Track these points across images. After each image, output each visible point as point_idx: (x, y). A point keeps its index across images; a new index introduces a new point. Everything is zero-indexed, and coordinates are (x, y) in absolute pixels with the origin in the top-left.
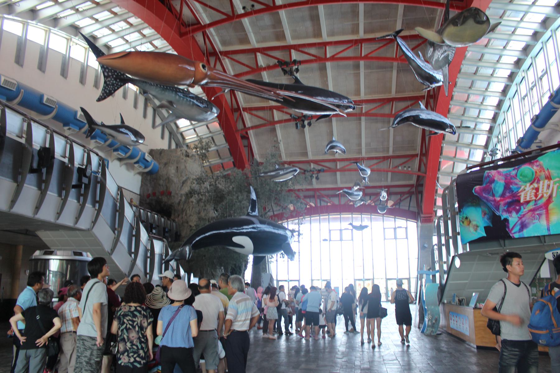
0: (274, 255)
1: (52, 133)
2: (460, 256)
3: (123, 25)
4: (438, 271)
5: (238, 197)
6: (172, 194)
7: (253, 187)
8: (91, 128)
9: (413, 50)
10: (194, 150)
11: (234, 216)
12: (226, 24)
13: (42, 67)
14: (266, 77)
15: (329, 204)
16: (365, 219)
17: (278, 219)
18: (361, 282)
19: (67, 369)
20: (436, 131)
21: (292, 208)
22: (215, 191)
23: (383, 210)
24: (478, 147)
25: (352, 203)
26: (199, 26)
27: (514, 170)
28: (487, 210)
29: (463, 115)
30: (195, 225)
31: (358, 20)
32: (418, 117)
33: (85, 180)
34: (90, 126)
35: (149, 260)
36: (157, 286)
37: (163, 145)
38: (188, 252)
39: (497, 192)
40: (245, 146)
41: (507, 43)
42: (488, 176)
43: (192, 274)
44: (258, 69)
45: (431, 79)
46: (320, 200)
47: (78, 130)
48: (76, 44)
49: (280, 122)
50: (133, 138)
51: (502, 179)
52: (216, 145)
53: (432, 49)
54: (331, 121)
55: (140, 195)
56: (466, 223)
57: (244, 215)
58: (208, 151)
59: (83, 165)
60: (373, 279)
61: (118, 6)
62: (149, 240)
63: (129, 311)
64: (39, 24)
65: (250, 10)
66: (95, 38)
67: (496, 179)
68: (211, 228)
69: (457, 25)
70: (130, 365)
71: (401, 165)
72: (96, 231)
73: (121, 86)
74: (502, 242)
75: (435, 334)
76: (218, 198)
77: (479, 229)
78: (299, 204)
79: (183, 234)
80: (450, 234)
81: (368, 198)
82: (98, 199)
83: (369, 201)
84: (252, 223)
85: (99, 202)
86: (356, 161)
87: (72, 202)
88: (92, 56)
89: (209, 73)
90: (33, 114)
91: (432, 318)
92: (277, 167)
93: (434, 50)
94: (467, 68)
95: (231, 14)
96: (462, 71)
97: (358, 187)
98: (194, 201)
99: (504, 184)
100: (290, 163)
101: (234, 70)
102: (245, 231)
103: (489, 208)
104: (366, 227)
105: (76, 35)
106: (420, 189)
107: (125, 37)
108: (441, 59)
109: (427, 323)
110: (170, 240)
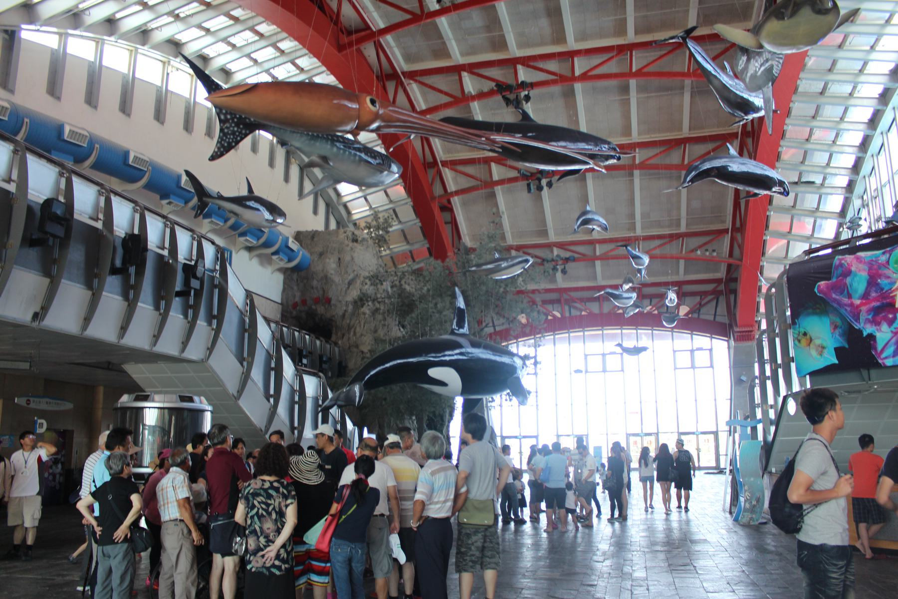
0: (497, 397)
1: (142, 211)
2: (795, 396)
3: (249, 36)
4: (760, 421)
5: (436, 304)
6: (333, 302)
7: (459, 288)
8: (202, 200)
9: (714, 59)
10: (366, 231)
11: (432, 336)
12: (412, 28)
13: (125, 107)
14: (478, 112)
15: (583, 313)
16: (642, 337)
17: (501, 339)
18: (638, 439)
19: (172, 576)
20: (757, 191)
21: (524, 321)
22: (400, 295)
23: (671, 321)
24: (829, 215)
25: (621, 311)
26: (368, 32)
27: (884, 253)
28: (838, 321)
29: (802, 162)
30: (370, 351)
31: (625, 13)
32: (727, 166)
33: (195, 284)
34: (200, 200)
35: (297, 407)
36: (310, 448)
37: (317, 223)
38: (358, 394)
39: (856, 291)
40: (446, 223)
41: (877, 40)
42: (841, 265)
43: (366, 429)
44: (463, 99)
45: (746, 107)
47: (183, 205)
48: (177, 69)
49: (501, 182)
50: (267, 215)
51: (864, 270)
52: (400, 222)
53: (745, 58)
54: (584, 179)
55: (281, 304)
56: (804, 342)
57: (446, 333)
58: (388, 232)
59: (191, 260)
60: (657, 434)
61: (240, 6)
63: (261, 488)
64: (119, 41)
66: (205, 59)
67: (853, 269)
68: (398, 354)
69: (783, 19)
70: (265, 571)
71: (700, 247)
72: (212, 362)
73: (246, 135)
74: (865, 373)
75: (757, 523)
76: (405, 306)
77: (825, 351)
78: (535, 314)
79: (351, 365)
80: (779, 361)
81: (647, 301)
82: (215, 312)
83: (649, 308)
84: (459, 346)
85: (217, 318)
86: (627, 242)
87: (176, 318)
88: (202, 93)
89: (381, 112)
90: (114, 183)
91: (751, 497)
92: (497, 255)
93: (748, 60)
94: (807, 84)
95: (418, 12)
96: (800, 90)
97: (630, 285)
98: (368, 312)
99: (867, 277)
100: (518, 248)
101: (425, 101)
102: (447, 358)
103: (843, 318)
104: (644, 349)
105: (176, 57)
106: (732, 285)
107: (252, 55)
108: (759, 73)
109: (743, 504)
110: (330, 374)
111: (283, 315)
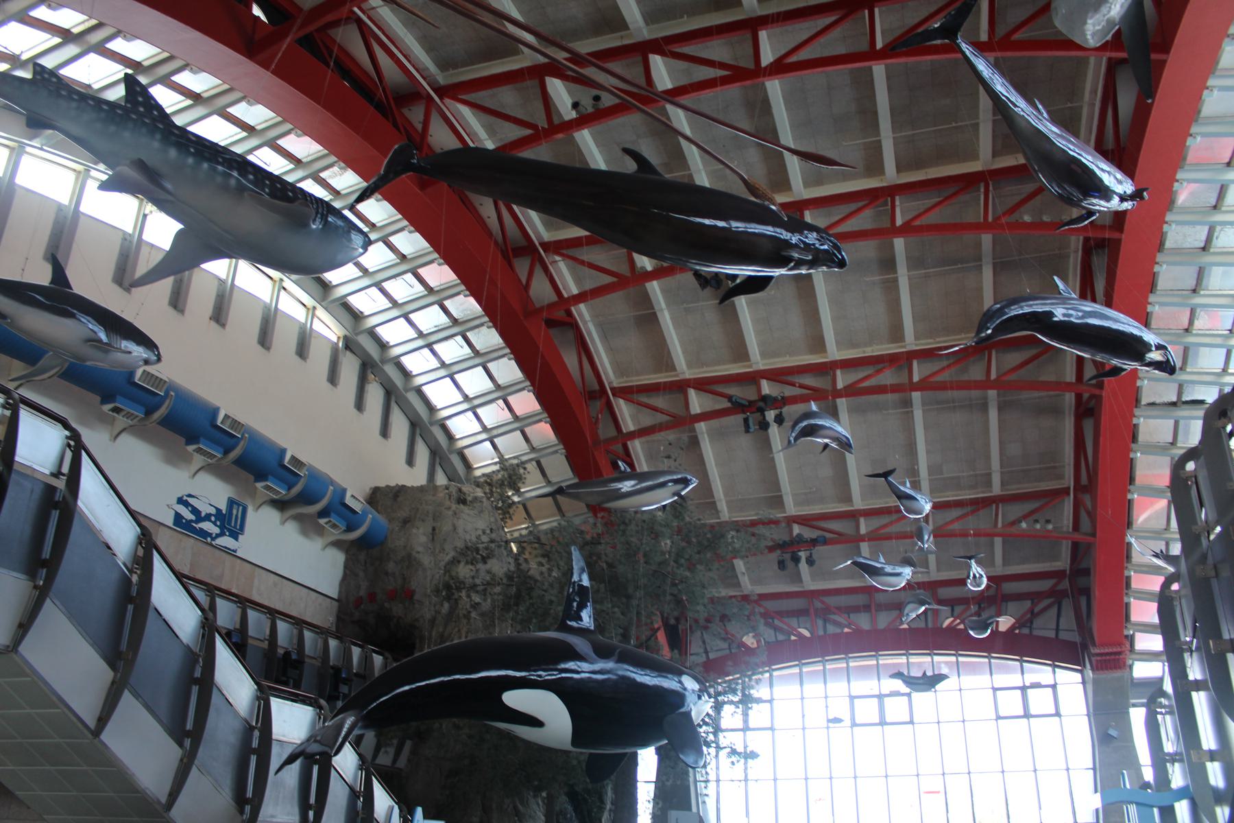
6: (417, 597)
15: (846, 630)
20: (1115, 362)
31: (878, 134)
43: (419, 810)
46: (825, 621)
62: (258, 698)
65: (590, 110)
71: (1025, 517)
101: (578, 281)
106: (1082, 582)
111: (339, 619)
